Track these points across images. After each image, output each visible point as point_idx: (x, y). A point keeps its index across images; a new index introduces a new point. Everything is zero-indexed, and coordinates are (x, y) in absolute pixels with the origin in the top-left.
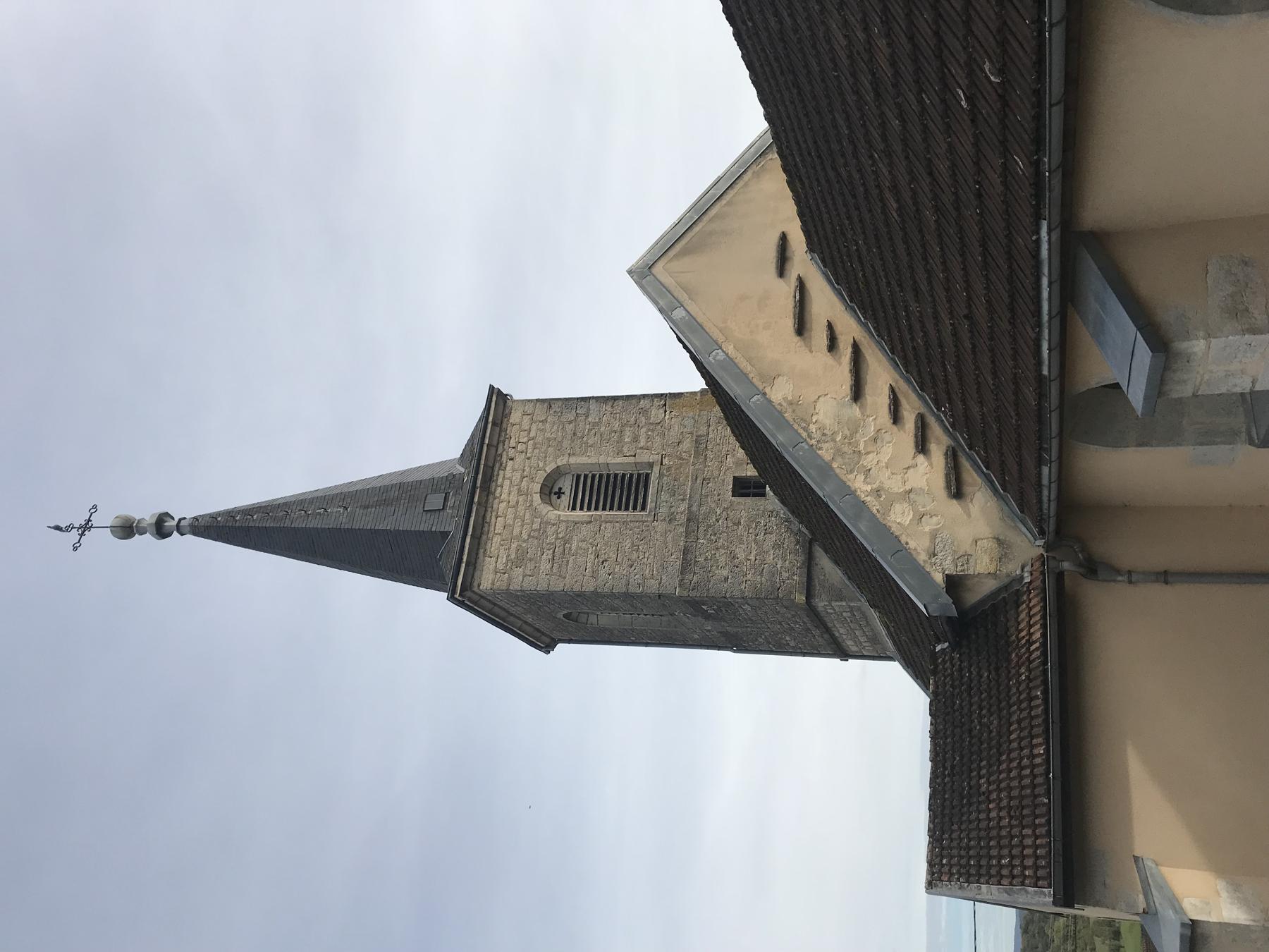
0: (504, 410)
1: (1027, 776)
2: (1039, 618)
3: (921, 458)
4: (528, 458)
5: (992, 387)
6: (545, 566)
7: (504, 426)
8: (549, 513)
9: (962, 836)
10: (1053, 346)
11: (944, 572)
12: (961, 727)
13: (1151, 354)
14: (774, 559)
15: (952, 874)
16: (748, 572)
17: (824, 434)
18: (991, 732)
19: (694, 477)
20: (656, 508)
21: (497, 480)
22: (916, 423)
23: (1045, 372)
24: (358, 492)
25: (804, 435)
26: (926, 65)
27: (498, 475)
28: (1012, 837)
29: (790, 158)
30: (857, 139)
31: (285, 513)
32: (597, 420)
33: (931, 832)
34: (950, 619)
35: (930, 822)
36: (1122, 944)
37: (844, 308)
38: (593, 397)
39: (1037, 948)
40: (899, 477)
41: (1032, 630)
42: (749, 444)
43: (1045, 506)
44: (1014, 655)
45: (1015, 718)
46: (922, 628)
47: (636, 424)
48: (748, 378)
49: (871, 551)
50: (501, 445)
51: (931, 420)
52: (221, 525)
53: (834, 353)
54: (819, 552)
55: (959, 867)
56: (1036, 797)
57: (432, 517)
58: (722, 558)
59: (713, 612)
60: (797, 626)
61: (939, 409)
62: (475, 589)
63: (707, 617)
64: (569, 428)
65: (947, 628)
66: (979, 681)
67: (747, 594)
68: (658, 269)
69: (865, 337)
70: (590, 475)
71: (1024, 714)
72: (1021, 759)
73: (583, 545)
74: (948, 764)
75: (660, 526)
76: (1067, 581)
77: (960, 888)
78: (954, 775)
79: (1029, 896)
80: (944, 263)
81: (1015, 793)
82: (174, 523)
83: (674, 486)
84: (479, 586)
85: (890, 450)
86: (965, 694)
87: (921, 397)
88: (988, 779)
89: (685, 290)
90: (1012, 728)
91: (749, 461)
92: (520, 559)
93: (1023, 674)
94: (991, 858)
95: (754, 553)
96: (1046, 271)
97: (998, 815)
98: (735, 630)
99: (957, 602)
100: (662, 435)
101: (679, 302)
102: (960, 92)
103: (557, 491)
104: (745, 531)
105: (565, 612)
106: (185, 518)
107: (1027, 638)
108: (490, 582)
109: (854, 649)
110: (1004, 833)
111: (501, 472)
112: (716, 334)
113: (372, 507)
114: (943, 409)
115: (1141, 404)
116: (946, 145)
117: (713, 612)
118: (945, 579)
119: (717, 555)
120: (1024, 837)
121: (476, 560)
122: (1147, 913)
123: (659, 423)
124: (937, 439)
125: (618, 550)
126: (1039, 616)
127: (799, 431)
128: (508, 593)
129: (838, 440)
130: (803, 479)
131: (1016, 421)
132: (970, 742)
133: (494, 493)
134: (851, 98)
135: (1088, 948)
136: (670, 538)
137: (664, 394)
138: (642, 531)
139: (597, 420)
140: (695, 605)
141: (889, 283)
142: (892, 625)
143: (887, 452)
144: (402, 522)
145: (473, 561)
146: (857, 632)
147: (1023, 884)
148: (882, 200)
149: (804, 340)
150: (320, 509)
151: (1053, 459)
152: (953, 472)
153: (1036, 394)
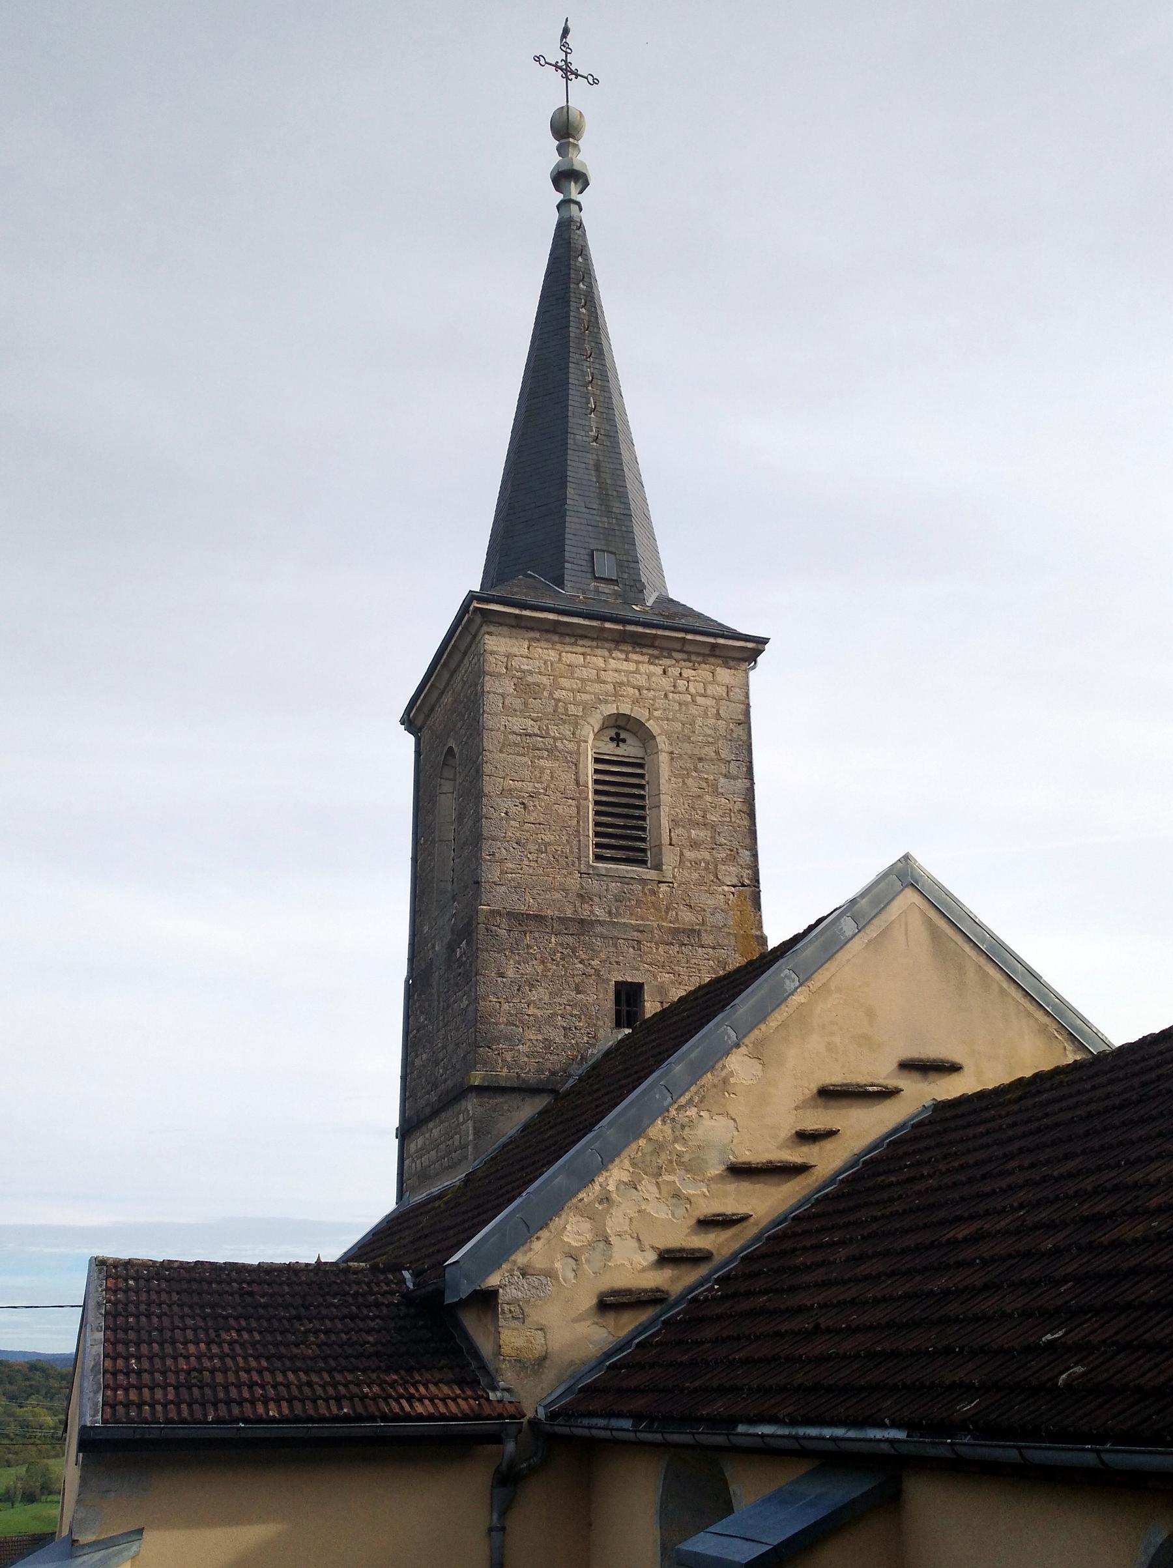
0: (734, 659)
1: (240, 1393)
2: (442, 1411)
3: (652, 1257)
4: (666, 696)
5: (730, 1358)
6: (518, 723)
7: (712, 660)
8: (589, 727)
9: (164, 1306)
10: (767, 1440)
11: (501, 1287)
12: (303, 1306)
13: (744, 1562)
14: (531, 1040)
15: (115, 1292)
16: (511, 1005)
17: (683, 1127)
18: (297, 1345)
19: (641, 929)
20: (598, 875)
21: (636, 653)
22: (700, 1250)
23: (741, 1429)
24: (617, 456)
25: (683, 1101)
26: (1102, 1289)
27: (642, 654)
28: (163, 1373)
29: (1048, 1085)
30: (1046, 1187)
31: (589, 352)
32: (720, 790)
33: (168, 1265)
34: (440, 1293)
35: (181, 1263)
36: (17, 1505)
37: (856, 1151)
38: (753, 784)
39: (11, 1383)
40: (626, 1228)
41: (426, 1402)
42: (684, 1011)
43: (586, 1422)
44: (395, 1377)
45: (315, 1378)
46: (433, 1252)
47: (715, 845)
48: (759, 1022)
49: (528, 1190)
50: (685, 656)
51: (703, 1270)
52: (572, 262)
53: (797, 1140)
54: (540, 1103)
55: (124, 1301)
56: (215, 1405)
57: (584, 563)
58: (532, 968)
59: (458, 955)
60: (441, 1071)
61: (717, 1281)
62: (485, 628)
63: (451, 947)
64: (709, 751)
65: (430, 1288)
66: (361, 1330)
67: (482, 1003)
68: (910, 896)
69: (816, 1180)
70: (644, 782)
71: (319, 1391)
72: (263, 1387)
73: (546, 777)
74: (255, 1288)
75: (573, 882)
76: (492, 1448)
77: (98, 1303)
78: (241, 1296)
79: (92, 1395)
80: (884, 1299)
81: (219, 1378)
82: (574, 195)
83: (630, 900)
84: (489, 633)
85: (664, 1216)
86: (345, 1311)
87: (735, 1255)
88: (236, 1342)
89: (884, 934)
90: (301, 1374)
91: (666, 1005)
92: (526, 689)
93: (370, 1388)
94: (138, 1344)
95: (539, 1013)
96: (852, 1434)
97: (191, 1355)
98: (434, 983)
99: (465, 1303)
100: (701, 883)
101: (864, 927)
102: (1061, 1333)
103: (621, 737)
104: (568, 1000)
105: (456, 750)
106: (581, 210)
107: (417, 1395)
108: (495, 649)
109: (413, 1147)
110: (169, 1362)
111: (646, 658)
112: (820, 978)
113: (598, 476)
114: (716, 1287)
115: (690, 1549)
116: (1009, 1311)
117: (458, 955)
118: (492, 1289)
119: (535, 962)
120: (164, 1388)
121: (524, 628)
122: (72, 1545)
123: (717, 878)
124: (678, 1278)
125: (540, 824)
126: (445, 1411)
127: (687, 1094)
128: (480, 673)
129: (676, 1146)
130: (630, 1092)
131: (688, 1387)
132: (284, 1317)
133: (616, 649)
134: (1088, 1184)
135: (11, 1456)
136: (557, 896)
137: (759, 883)
138: (567, 858)
139: (720, 790)
140: (466, 930)
141: (875, 1219)
142: (442, 1205)
143: (660, 1211)
144: (577, 520)
145: (523, 624)
146: (433, 1153)
147: (106, 1387)
148: (971, 1218)
149: (812, 1098)
150: (595, 403)
151: (638, 1434)
152: (633, 1299)
153: (715, 1415)
